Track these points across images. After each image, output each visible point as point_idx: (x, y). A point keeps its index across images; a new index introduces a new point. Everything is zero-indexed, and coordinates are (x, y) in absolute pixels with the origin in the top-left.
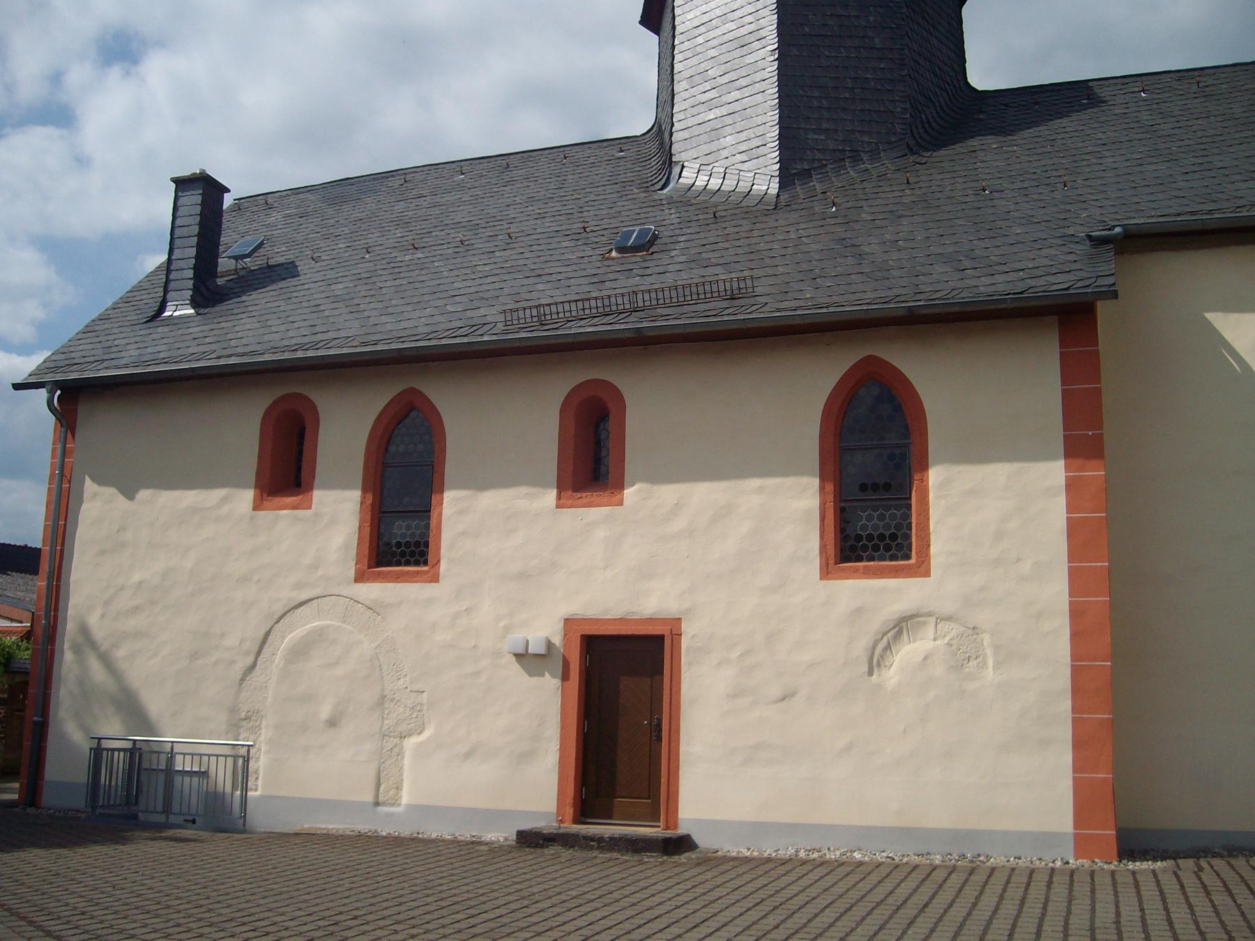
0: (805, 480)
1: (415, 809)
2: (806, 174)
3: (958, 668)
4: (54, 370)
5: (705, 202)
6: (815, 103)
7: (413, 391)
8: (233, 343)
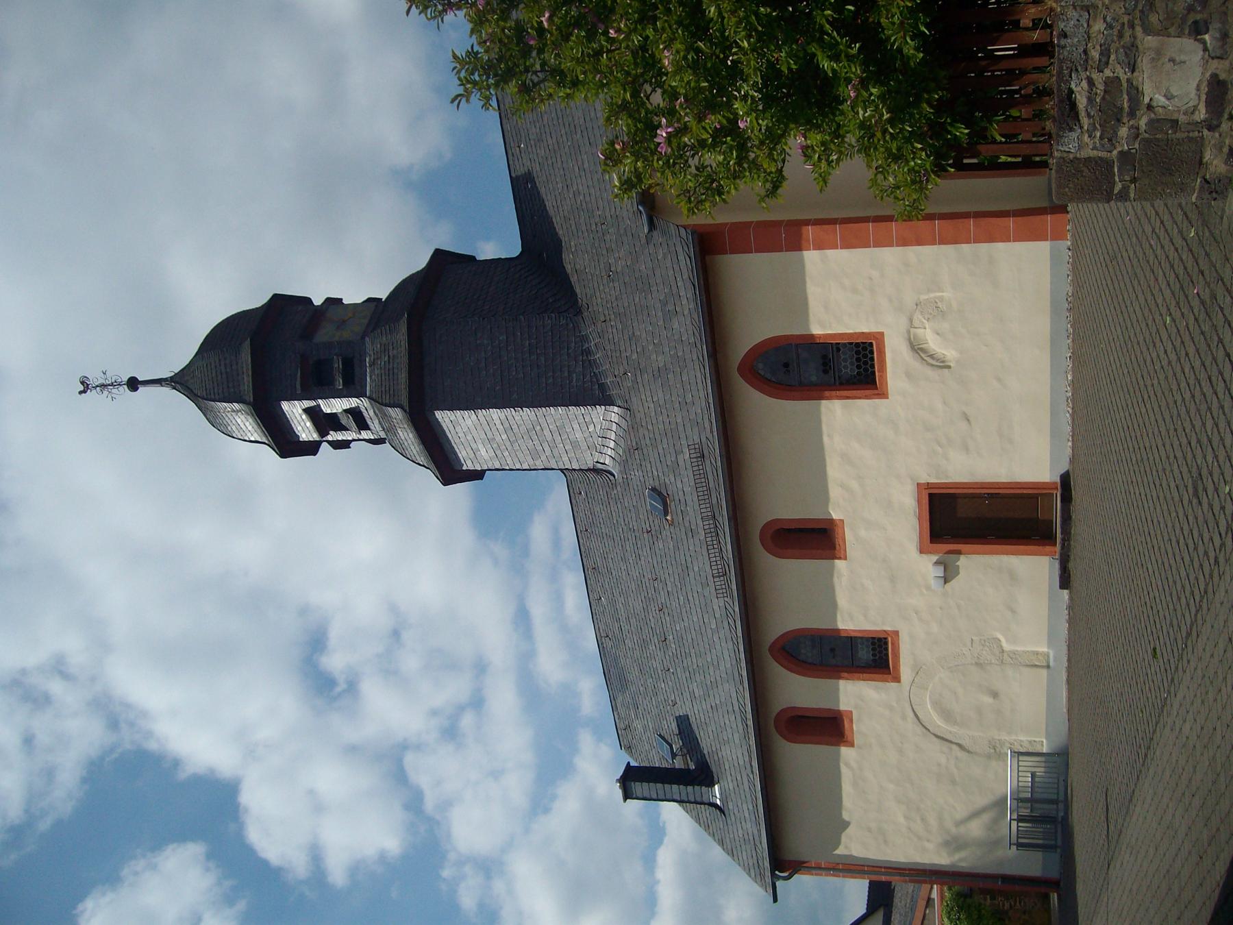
0: (823, 409)
1: (1051, 641)
2: (602, 387)
3: (943, 314)
4: (762, 876)
5: (624, 452)
6: (551, 381)
7: (771, 649)
8: (741, 763)
